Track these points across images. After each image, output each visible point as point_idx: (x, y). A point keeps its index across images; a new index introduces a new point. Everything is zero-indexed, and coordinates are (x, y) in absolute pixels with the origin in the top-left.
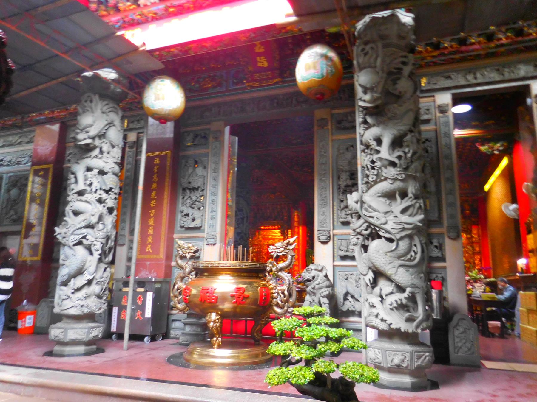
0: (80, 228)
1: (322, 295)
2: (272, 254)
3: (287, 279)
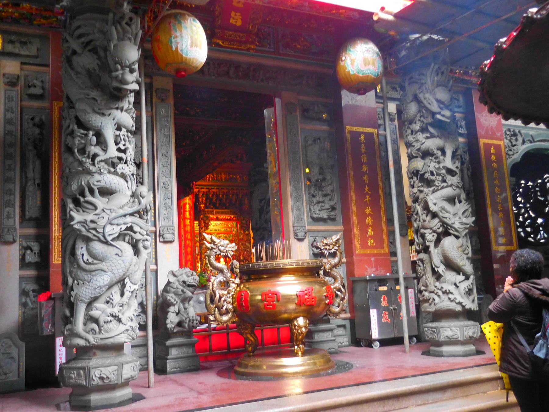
0: (125, 216)
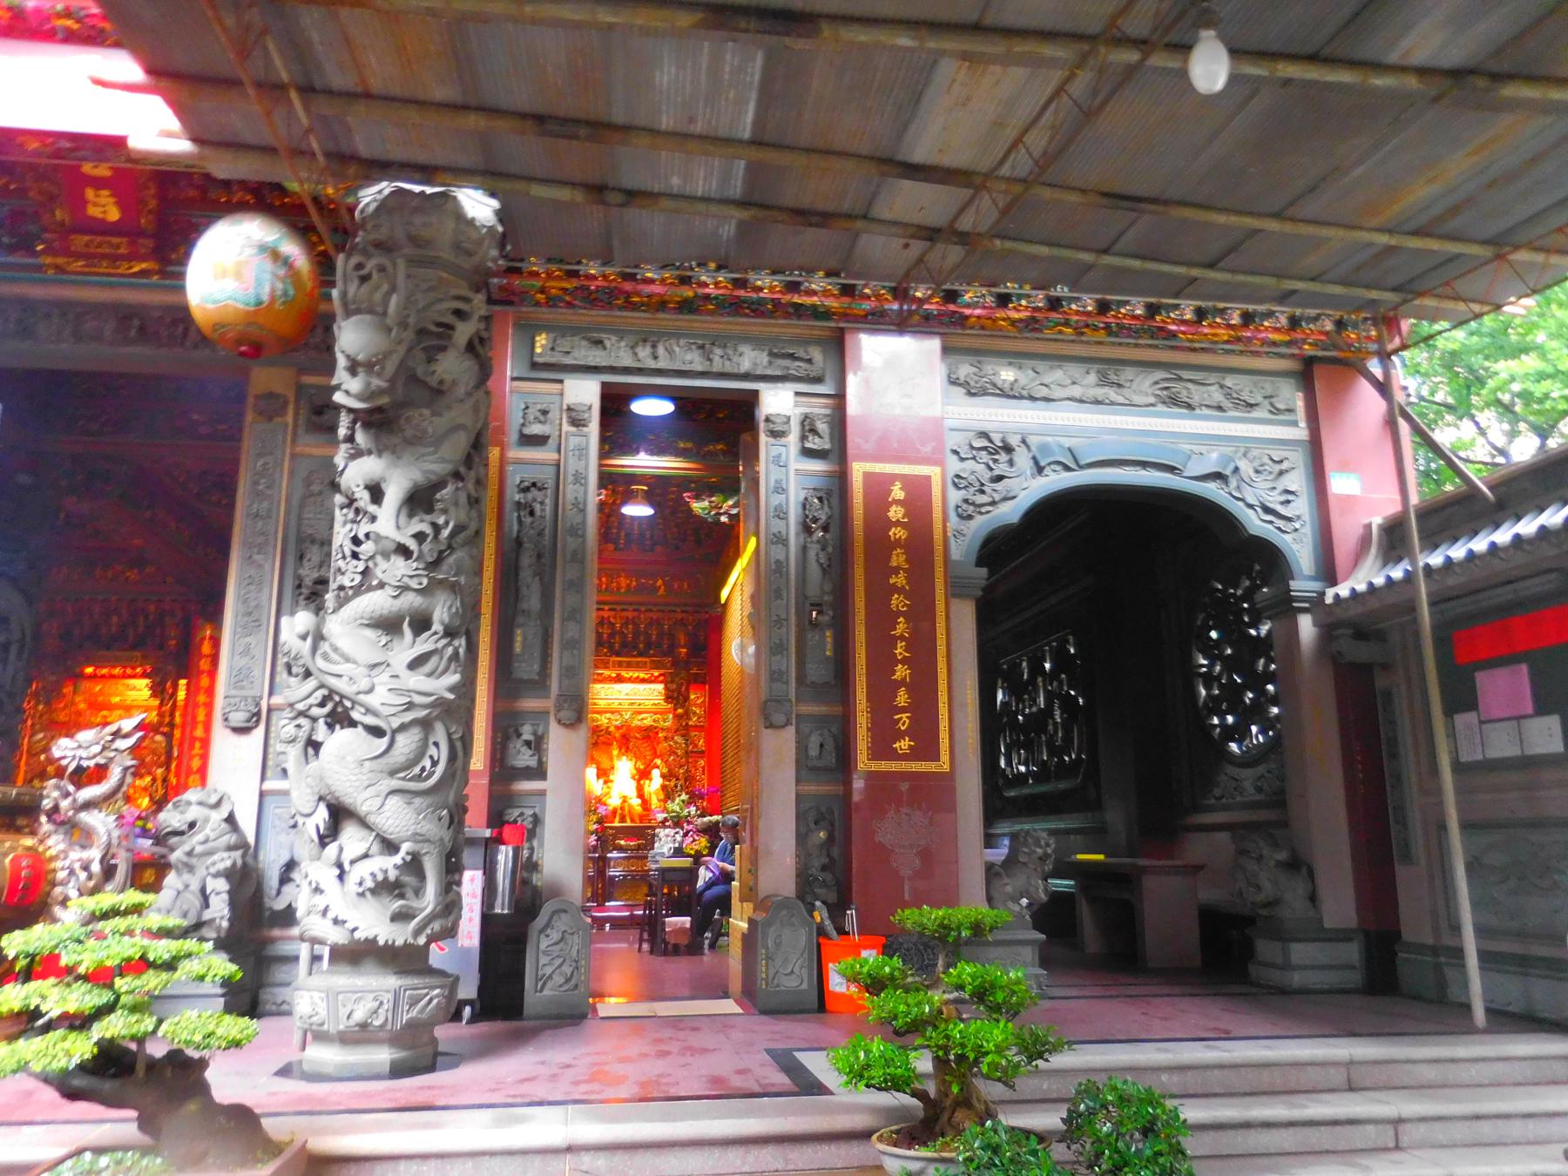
1: (213, 870)
2: (64, 762)
3: (101, 830)
